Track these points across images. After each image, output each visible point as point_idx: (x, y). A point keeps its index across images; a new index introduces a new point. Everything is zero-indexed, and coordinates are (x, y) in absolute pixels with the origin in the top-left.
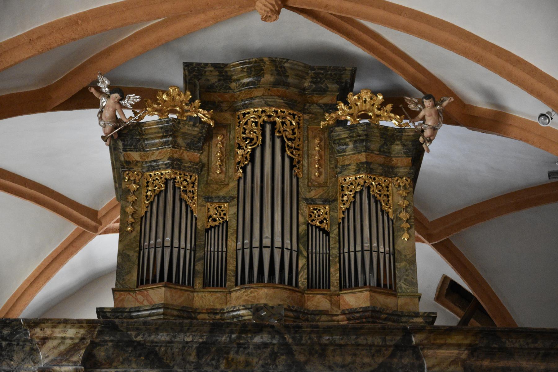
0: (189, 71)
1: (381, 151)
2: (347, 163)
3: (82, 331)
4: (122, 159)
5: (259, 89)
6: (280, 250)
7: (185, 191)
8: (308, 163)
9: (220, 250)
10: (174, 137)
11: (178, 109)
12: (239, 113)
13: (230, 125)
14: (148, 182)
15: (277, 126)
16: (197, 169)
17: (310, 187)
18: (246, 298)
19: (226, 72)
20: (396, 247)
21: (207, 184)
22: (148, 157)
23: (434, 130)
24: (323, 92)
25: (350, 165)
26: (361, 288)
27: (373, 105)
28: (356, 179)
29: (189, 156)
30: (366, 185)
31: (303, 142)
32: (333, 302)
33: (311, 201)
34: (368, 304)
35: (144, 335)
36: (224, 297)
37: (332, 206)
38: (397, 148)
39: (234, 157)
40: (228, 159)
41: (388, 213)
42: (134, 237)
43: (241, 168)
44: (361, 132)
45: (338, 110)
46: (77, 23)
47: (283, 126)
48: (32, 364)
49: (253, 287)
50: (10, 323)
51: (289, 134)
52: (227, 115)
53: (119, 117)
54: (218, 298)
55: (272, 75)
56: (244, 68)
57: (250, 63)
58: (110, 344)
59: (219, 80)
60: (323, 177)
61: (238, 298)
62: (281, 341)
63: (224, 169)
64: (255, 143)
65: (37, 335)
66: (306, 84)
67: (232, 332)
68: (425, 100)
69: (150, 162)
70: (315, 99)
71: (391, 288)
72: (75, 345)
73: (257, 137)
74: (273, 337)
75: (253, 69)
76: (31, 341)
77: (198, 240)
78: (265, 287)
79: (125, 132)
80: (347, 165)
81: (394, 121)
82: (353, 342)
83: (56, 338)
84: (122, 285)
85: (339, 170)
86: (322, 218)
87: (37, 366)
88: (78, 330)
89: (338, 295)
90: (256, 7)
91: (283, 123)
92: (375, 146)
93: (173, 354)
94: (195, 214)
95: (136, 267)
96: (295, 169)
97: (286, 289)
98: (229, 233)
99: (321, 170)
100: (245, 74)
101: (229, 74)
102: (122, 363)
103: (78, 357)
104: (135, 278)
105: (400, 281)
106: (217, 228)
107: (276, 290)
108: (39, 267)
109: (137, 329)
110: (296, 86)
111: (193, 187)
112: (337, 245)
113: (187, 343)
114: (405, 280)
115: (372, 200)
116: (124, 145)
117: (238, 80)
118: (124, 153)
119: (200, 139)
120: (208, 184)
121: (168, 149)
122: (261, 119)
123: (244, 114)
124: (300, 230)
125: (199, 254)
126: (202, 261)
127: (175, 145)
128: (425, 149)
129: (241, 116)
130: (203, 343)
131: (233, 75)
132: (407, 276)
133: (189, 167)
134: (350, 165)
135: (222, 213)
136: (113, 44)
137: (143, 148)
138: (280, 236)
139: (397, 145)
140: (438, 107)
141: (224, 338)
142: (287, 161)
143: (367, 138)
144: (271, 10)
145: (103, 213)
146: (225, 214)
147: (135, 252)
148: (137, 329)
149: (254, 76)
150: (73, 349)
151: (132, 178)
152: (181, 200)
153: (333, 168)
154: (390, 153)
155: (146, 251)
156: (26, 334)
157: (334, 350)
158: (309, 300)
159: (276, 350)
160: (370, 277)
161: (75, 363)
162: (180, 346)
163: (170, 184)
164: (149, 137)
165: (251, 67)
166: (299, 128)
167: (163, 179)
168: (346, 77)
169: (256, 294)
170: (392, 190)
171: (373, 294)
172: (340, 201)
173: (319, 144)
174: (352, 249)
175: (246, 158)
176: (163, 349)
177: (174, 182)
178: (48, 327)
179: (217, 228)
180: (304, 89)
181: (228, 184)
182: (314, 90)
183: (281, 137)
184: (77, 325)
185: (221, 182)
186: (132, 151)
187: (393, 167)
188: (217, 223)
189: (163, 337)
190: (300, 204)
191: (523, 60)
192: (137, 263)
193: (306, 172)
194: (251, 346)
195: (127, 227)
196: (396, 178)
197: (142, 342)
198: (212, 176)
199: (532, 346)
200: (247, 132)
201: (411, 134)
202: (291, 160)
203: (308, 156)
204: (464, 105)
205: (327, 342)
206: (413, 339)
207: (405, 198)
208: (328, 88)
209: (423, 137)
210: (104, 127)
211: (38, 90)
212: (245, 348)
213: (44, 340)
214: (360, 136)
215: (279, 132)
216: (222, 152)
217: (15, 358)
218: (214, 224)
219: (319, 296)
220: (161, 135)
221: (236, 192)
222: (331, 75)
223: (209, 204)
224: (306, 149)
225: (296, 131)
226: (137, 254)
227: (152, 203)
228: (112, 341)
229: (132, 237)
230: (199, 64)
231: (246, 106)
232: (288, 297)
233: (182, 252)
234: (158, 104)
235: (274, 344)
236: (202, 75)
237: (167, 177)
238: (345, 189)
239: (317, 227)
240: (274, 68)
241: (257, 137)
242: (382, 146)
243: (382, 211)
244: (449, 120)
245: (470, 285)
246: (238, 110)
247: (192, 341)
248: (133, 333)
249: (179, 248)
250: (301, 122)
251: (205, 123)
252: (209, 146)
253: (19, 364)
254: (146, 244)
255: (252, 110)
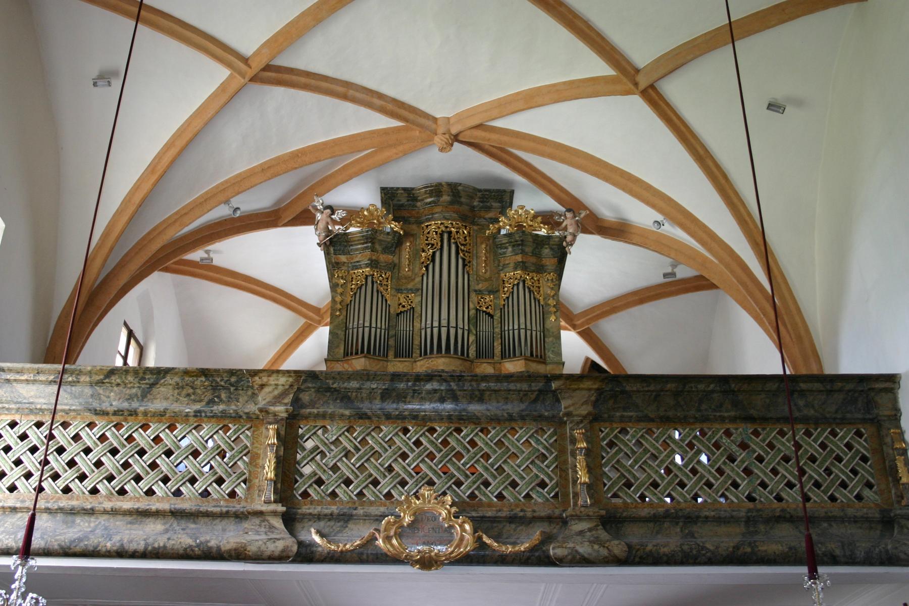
0: (384, 194)
1: (534, 254)
2: (507, 262)
3: (291, 380)
4: (333, 261)
5: (438, 207)
6: (455, 329)
7: (381, 285)
8: (477, 263)
9: (408, 329)
10: (373, 243)
11: (375, 221)
12: (423, 225)
13: (416, 234)
14: (352, 278)
15: (453, 235)
16: (390, 268)
17: (478, 281)
18: (428, 365)
19: (413, 194)
20: (545, 326)
21: (398, 279)
22: (352, 259)
23: (575, 236)
24: (489, 209)
25: (509, 264)
26: (518, 357)
27: (527, 218)
28: (514, 274)
29: (384, 258)
30: (522, 279)
31: (473, 247)
32: (496, 369)
33: (479, 292)
34: (523, 369)
35: (339, 383)
36: (411, 366)
37: (496, 295)
38: (546, 251)
39: (419, 258)
40: (414, 260)
41: (539, 301)
42: (342, 320)
43: (425, 267)
44: (518, 238)
45: (499, 221)
46: (298, 156)
47: (457, 234)
48: (254, 405)
49: (433, 357)
50: (235, 373)
51: (462, 240)
52: (414, 227)
53: (330, 228)
54: (406, 366)
55: (449, 195)
56: (427, 191)
57: (431, 186)
58: (313, 390)
59: (408, 201)
60: (488, 273)
61: (422, 366)
62: (448, 388)
63: (411, 268)
64: (436, 248)
65: (257, 382)
66: (475, 204)
67: (408, 381)
68: (566, 213)
69: (355, 262)
70: (482, 214)
71: (541, 357)
72: (287, 390)
73: (437, 243)
74: (441, 385)
75: (434, 191)
76: (252, 387)
77: (390, 322)
78: (442, 357)
79: (335, 240)
80: (507, 264)
81: (543, 230)
82: (505, 388)
83: (271, 385)
84: (332, 356)
85: (501, 268)
86: (488, 304)
87: (257, 407)
88: (287, 379)
89: (500, 363)
90: (435, 142)
91: (457, 232)
92: (528, 249)
93: (362, 398)
94: (388, 302)
95: (343, 342)
96: (467, 267)
97: (459, 358)
98: (415, 317)
99: (487, 268)
100: (428, 195)
101: (415, 195)
102: (322, 405)
103: (288, 399)
104: (342, 351)
105: (549, 352)
106: (405, 313)
107: (451, 359)
108: (278, 352)
109: (333, 378)
110: (467, 205)
111: (387, 281)
112: (500, 325)
113: (373, 389)
114: (553, 351)
115: (527, 290)
116: (334, 250)
117: (422, 200)
118: (334, 256)
119: (393, 245)
120: (399, 279)
121: (368, 253)
122: (441, 230)
123: (427, 226)
124: (471, 314)
125: (392, 333)
126: (394, 338)
127: (373, 250)
128: (568, 251)
129: (425, 228)
130: (385, 389)
131: (418, 196)
132: (554, 348)
133: (384, 266)
134: (509, 264)
135: (410, 301)
136: (327, 174)
137: (349, 253)
138: (455, 319)
139: (546, 248)
140: (577, 218)
141: (402, 386)
142: (460, 261)
143: (523, 243)
144: (446, 143)
145: (325, 310)
146: (412, 302)
147: (342, 331)
148: (333, 378)
149: (434, 197)
150: (284, 394)
151: (340, 275)
152: (378, 291)
153: (496, 267)
154: (541, 255)
155: (351, 331)
156: (248, 382)
157: (490, 395)
158: (477, 367)
159: (444, 395)
160: (525, 349)
161: (286, 404)
162: (368, 392)
163: (370, 279)
164: (353, 243)
165: (432, 190)
166: (470, 236)
167: (364, 276)
168: (507, 198)
169: (435, 362)
170: (542, 282)
171: (527, 362)
172: (501, 292)
173: (485, 248)
174: (511, 328)
175: (428, 259)
176: (354, 394)
177: (373, 278)
178: (264, 376)
179: (405, 313)
180: (474, 207)
181: (414, 279)
182: (482, 207)
183: (456, 243)
184: (287, 375)
185: (409, 277)
186: (340, 254)
187: (543, 266)
188: (406, 309)
189: (354, 384)
190: (471, 295)
191: (641, 179)
192: (344, 339)
193: (475, 269)
194: (424, 392)
195: (336, 312)
196: (545, 274)
197: (338, 389)
198: (402, 273)
199: (646, 389)
200: (429, 239)
201: (557, 240)
202: (464, 260)
203: (477, 257)
204: (598, 219)
205: (484, 388)
206: (553, 385)
207: (552, 289)
208: (492, 205)
209: (566, 241)
210: (319, 236)
211: (272, 211)
212: (419, 393)
213: (262, 386)
214: (517, 241)
215: (454, 239)
216: (410, 255)
217: (241, 400)
218: (403, 309)
219: (485, 364)
220: (362, 242)
221: (421, 285)
222: (494, 196)
223: (399, 294)
224: (475, 252)
225: (467, 238)
226: (343, 333)
227: (355, 294)
228: (314, 388)
229: (340, 320)
230: (392, 188)
231: (429, 220)
232: (461, 365)
233: (378, 330)
234: (361, 218)
235: (442, 390)
236: (394, 196)
237: (367, 274)
238: (505, 282)
239: (484, 312)
240: (450, 190)
241: (437, 243)
242: (534, 249)
243: (535, 299)
244: (585, 231)
245: (606, 362)
246: (422, 223)
247: (377, 388)
248: (331, 382)
249: (376, 328)
250: (472, 232)
251: (396, 232)
252: (400, 251)
253: (244, 404)
254: (351, 325)
255: (434, 222)
